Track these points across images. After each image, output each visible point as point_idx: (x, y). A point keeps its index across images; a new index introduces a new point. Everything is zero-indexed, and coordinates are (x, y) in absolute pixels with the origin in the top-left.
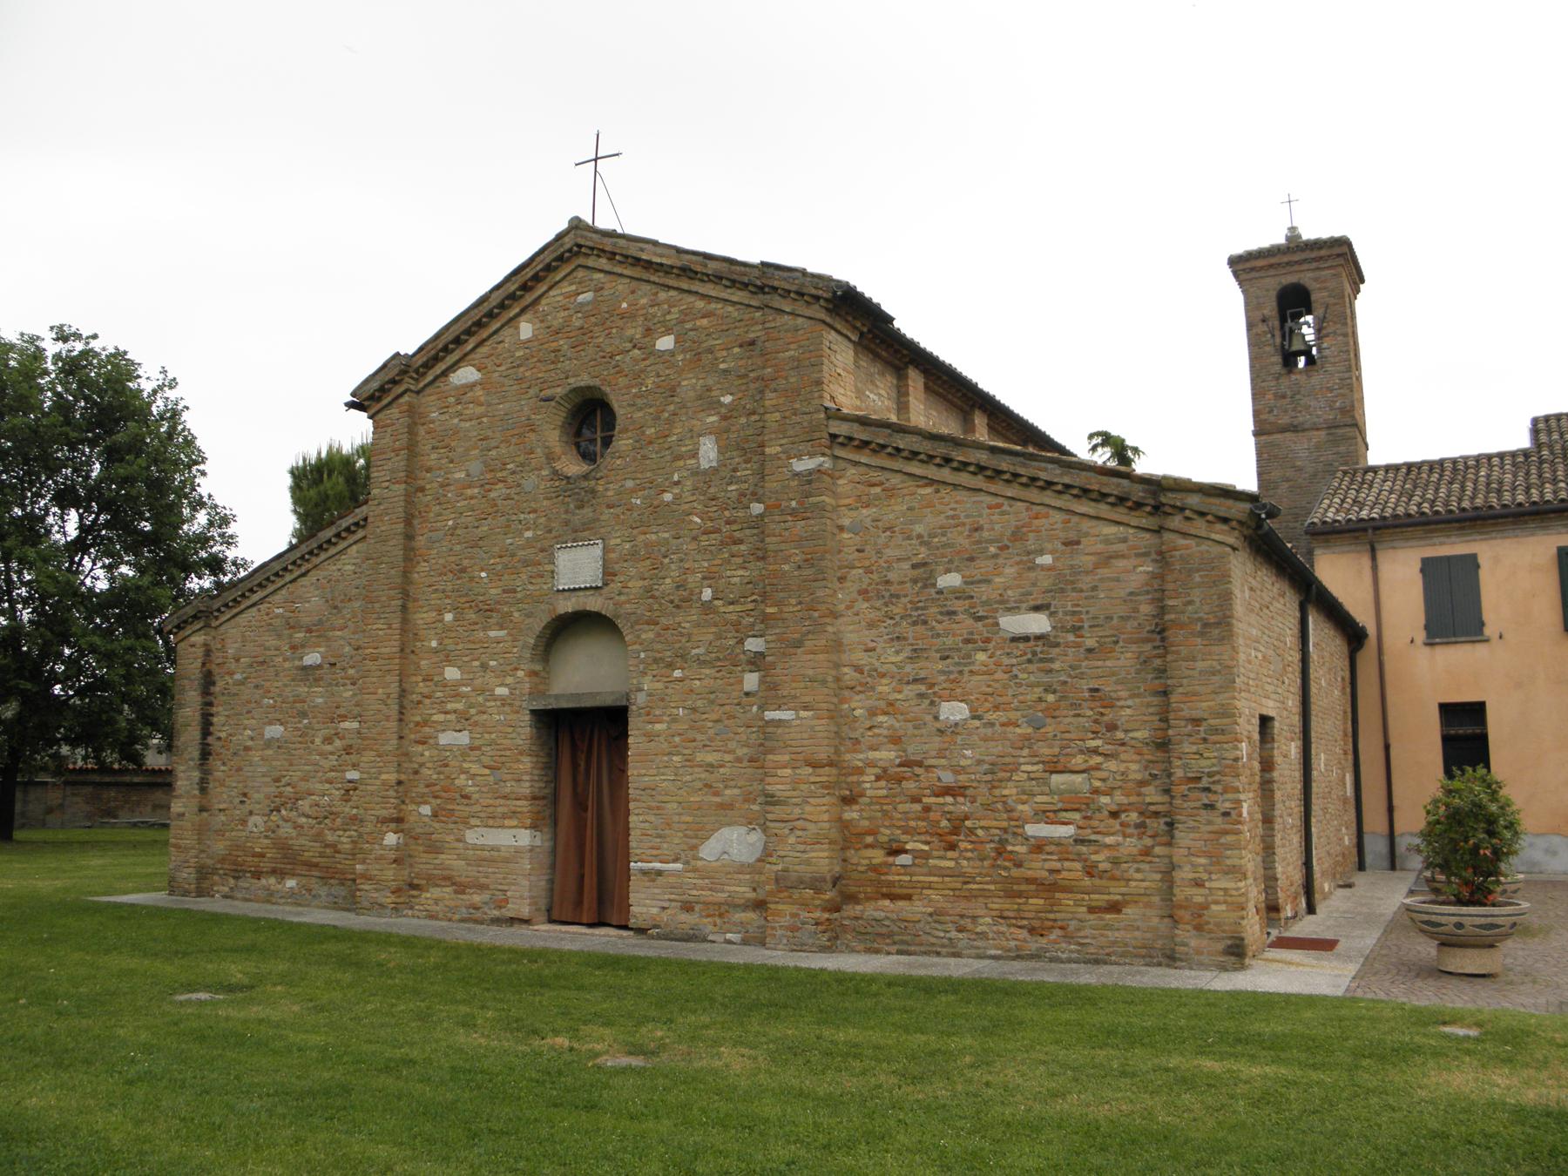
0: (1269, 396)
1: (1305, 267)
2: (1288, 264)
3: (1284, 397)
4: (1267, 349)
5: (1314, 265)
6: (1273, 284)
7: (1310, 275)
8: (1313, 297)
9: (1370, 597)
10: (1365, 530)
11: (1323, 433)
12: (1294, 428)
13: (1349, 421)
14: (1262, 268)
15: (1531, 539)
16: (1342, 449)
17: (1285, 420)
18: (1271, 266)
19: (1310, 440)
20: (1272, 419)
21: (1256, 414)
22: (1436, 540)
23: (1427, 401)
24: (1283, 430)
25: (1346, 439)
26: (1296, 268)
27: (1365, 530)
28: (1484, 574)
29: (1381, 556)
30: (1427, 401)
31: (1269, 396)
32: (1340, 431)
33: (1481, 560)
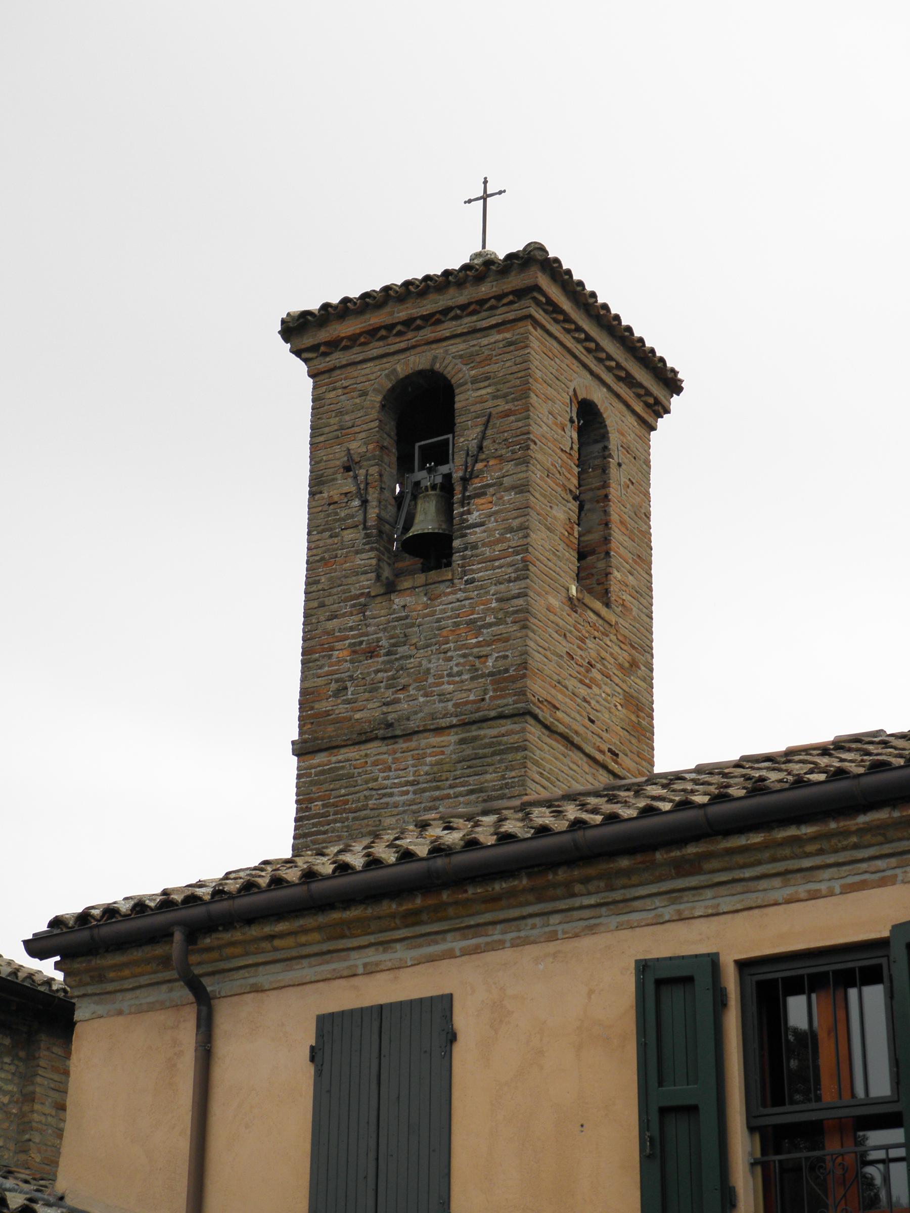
0: (341, 653)
1: (448, 328)
2: (408, 323)
3: (371, 653)
4: (349, 535)
5: (468, 322)
6: (376, 375)
7: (458, 347)
8: (460, 402)
9: (184, 1145)
10: (161, 935)
11: (451, 738)
12: (388, 732)
13: (509, 703)
14: (353, 340)
15: (587, 942)
16: (491, 778)
17: (369, 712)
18: (373, 333)
19: (420, 758)
20: (341, 710)
21: (307, 698)
22: (358, 960)
23: (754, 643)
24: (364, 738)
25: (500, 750)
26: (428, 333)
27: (161, 935)
28: (465, 1059)
29: (231, 1019)
30: (754, 643)
31: (341, 653)
32: (488, 732)
33: (462, 1020)
